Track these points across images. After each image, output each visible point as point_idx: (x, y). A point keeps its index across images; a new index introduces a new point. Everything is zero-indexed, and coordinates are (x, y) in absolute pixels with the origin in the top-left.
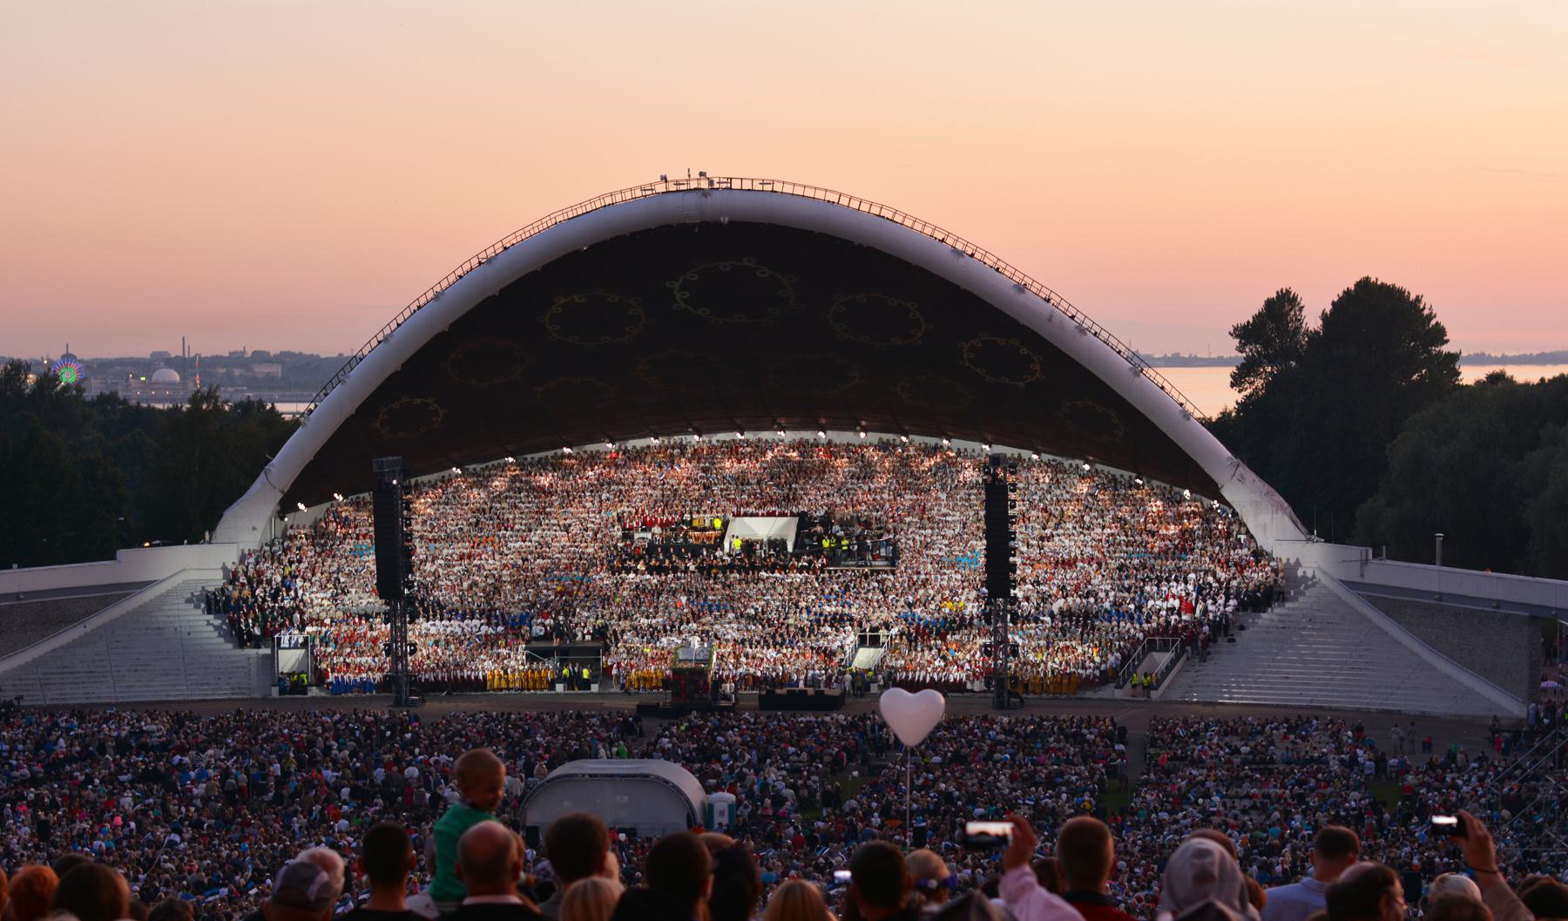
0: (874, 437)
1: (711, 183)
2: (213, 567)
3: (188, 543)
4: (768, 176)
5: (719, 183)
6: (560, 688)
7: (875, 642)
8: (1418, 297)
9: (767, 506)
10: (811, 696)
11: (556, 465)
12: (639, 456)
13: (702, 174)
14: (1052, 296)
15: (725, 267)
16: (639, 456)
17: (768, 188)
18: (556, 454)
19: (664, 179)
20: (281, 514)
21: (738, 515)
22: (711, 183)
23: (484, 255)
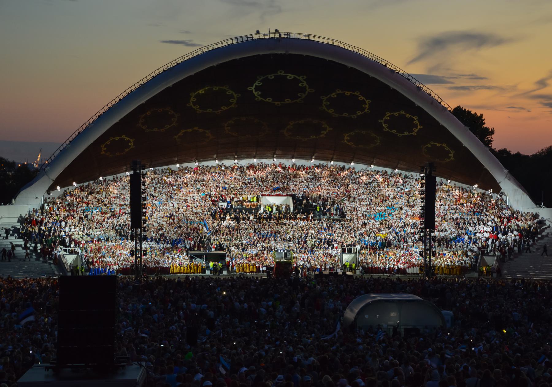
0: (318, 162)
1: (280, 35)
2: (15, 217)
3: (3, 205)
4: (307, 33)
5: (285, 35)
6: (208, 273)
7: (350, 251)
8: (481, 114)
9: (275, 191)
10: (340, 275)
11: (172, 173)
12: (209, 170)
13: (276, 30)
14: (432, 93)
15: (271, 77)
16: (209, 170)
17: (307, 38)
18: (169, 167)
19: (258, 32)
20: (48, 192)
21: (263, 195)
22: (280, 35)
23: (166, 66)
